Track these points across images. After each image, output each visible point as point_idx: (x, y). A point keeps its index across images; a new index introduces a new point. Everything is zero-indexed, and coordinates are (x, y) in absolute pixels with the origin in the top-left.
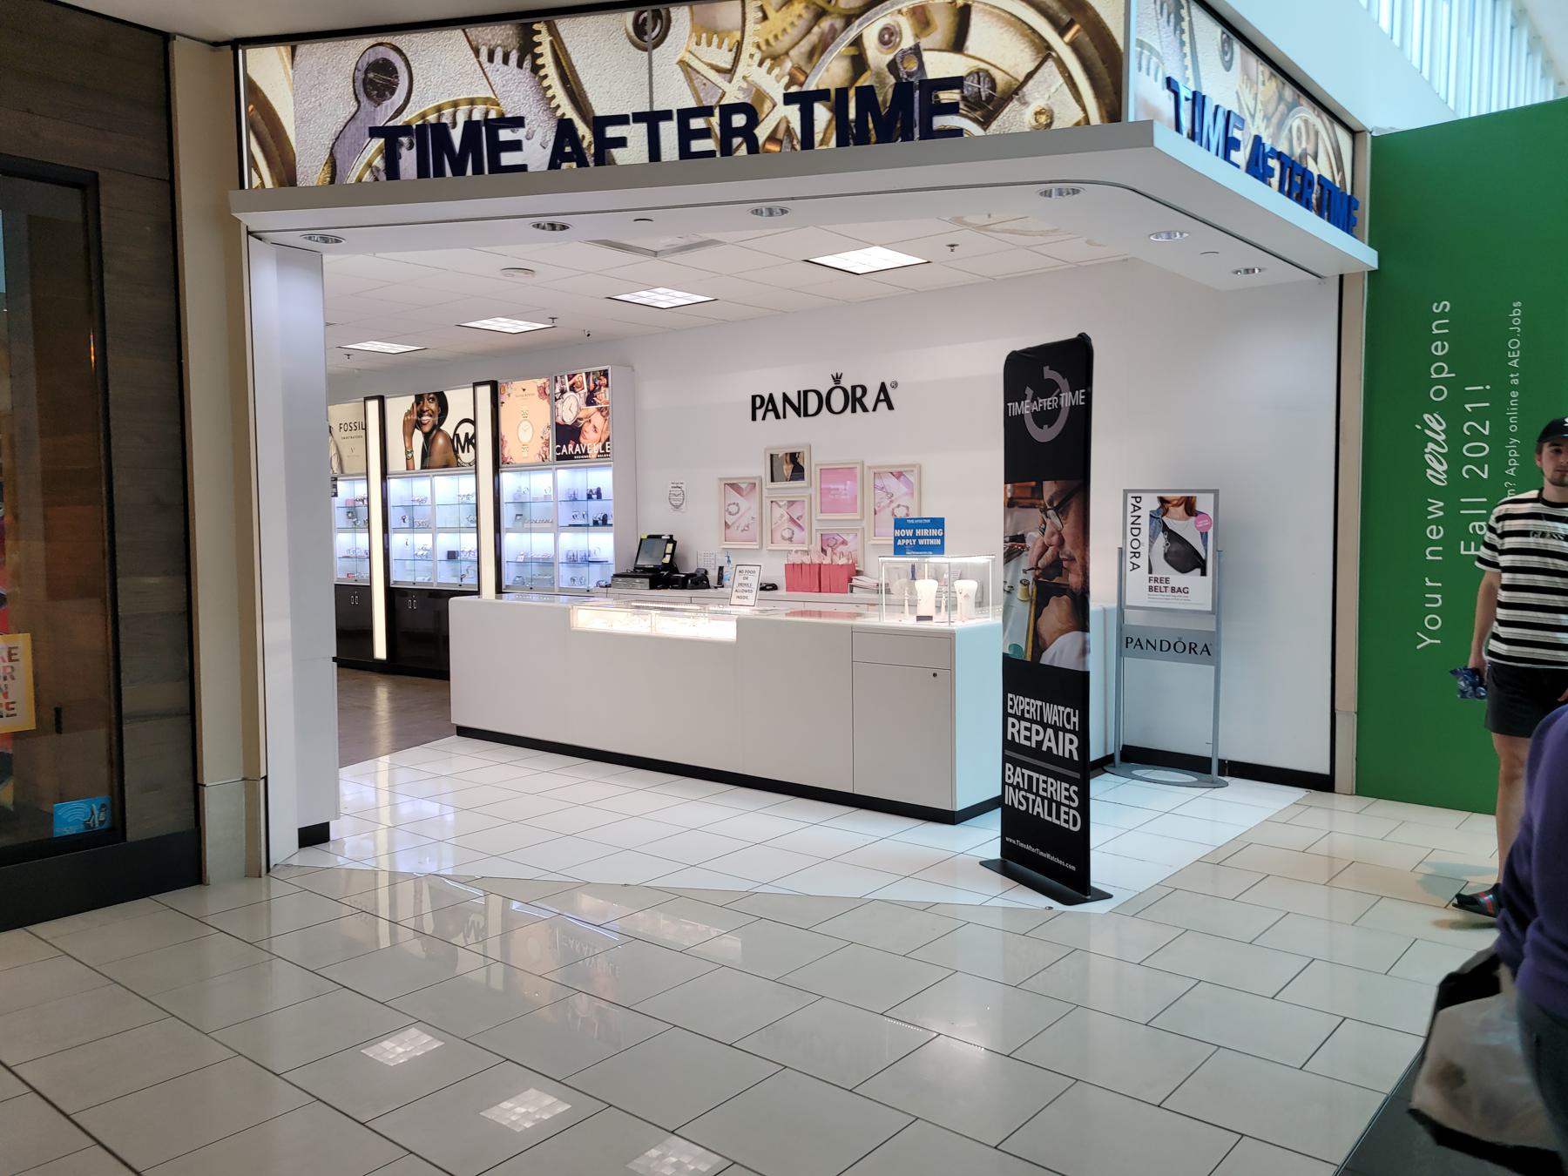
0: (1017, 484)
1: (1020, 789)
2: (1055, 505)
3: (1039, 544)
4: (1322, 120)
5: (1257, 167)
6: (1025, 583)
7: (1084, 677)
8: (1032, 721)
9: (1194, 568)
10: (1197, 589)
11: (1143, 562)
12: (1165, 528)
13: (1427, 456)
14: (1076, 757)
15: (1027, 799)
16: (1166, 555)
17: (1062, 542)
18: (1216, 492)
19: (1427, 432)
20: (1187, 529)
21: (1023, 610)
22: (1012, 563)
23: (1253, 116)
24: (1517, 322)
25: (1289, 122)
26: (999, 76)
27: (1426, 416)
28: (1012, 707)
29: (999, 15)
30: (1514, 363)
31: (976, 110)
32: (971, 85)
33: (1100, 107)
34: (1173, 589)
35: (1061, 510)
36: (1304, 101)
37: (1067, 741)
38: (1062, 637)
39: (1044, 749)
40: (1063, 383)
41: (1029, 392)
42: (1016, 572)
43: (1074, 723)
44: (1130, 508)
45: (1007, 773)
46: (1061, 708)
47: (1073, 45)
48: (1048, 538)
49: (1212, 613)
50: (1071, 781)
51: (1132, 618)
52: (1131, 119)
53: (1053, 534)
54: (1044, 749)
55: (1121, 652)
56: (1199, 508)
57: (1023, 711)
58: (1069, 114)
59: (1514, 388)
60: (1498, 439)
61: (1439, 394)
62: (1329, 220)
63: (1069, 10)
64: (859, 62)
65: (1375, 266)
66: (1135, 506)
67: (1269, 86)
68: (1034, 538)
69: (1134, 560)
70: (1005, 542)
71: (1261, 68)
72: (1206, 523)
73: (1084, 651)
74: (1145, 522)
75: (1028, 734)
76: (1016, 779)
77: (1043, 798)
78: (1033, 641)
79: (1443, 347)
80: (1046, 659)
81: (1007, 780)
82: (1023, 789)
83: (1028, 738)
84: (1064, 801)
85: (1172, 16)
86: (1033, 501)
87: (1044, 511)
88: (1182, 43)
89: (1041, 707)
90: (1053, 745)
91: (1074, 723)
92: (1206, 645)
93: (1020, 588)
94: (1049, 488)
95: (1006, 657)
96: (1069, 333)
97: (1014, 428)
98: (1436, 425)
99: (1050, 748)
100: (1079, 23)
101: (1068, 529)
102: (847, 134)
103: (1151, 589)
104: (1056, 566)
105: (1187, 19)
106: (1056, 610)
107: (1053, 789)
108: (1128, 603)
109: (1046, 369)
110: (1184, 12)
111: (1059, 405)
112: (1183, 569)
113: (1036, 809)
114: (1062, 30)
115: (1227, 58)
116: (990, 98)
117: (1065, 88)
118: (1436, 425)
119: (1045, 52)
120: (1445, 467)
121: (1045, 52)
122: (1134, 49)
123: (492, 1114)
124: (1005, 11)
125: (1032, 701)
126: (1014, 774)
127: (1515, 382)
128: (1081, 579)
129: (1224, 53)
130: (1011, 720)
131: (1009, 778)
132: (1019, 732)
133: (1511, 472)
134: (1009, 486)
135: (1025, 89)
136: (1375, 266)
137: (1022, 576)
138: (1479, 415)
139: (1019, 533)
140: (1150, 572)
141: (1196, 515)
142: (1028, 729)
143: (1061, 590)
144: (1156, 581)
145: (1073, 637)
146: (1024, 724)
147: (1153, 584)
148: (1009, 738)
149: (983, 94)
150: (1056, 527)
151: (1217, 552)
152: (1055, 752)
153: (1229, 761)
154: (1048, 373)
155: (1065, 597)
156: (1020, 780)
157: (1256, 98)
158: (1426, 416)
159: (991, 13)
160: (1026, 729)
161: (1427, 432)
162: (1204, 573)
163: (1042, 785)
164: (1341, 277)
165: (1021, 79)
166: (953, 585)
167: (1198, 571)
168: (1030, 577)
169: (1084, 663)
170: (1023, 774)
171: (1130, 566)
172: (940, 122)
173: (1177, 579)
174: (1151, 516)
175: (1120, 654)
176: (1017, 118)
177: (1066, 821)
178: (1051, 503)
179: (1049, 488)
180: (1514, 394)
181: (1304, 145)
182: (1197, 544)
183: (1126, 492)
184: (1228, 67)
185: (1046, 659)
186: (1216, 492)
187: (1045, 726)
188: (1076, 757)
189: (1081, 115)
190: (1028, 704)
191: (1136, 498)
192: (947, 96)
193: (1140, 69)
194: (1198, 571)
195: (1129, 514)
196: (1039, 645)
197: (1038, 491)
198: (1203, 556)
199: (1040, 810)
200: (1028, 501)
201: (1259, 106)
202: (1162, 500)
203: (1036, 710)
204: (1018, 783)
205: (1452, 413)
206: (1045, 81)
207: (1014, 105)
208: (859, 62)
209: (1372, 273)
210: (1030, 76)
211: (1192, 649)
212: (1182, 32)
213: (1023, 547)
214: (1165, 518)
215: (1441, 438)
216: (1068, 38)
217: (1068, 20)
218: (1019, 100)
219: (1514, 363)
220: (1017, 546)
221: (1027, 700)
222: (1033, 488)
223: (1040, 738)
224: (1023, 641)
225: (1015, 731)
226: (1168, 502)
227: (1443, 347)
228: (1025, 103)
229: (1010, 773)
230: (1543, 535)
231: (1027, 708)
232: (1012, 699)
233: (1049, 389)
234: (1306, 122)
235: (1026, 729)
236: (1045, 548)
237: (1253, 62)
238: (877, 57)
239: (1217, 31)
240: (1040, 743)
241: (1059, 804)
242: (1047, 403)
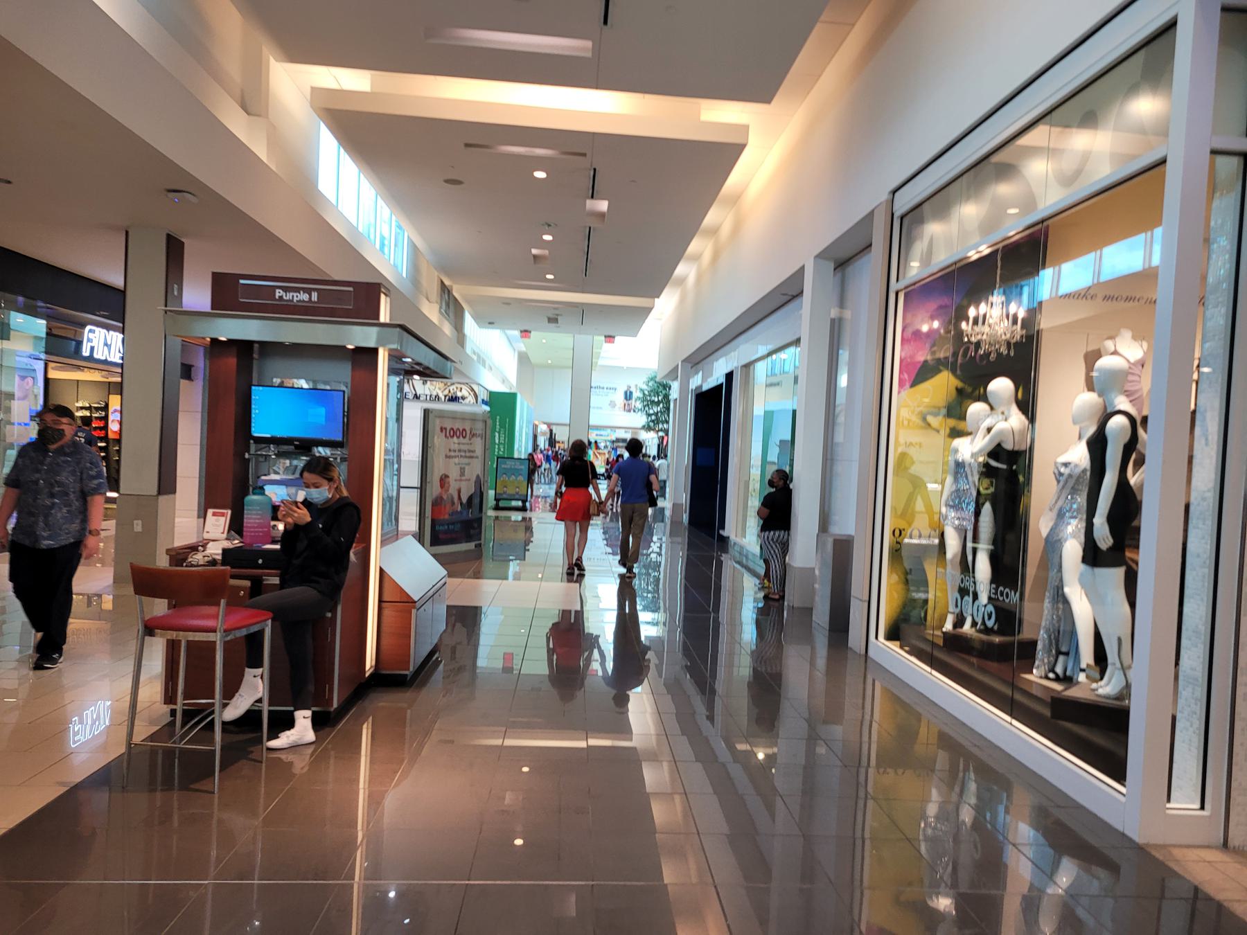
61: (497, 430)
64: (450, 392)
98: (497, 434)
102: (449, 400)
123: (356, 561)
166: (607, 470)
176: (467, 401)
205: (499, 433)
208: (450, 392)
213: (452, 515)
238: (452, 391)
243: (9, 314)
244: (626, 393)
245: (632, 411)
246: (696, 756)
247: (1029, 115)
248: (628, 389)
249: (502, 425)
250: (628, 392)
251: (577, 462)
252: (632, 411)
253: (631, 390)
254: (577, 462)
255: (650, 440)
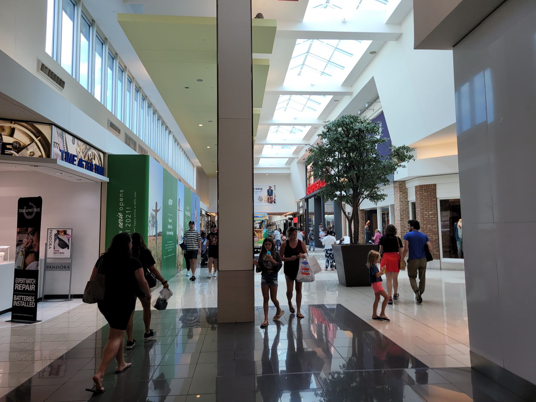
0: (21, 228)
1: (18, 301)
2: (31, 233)
3: (26, 242)
4: (96, 151)
5: (80, 164)
6: (22, 251)
7: (37, 271)
8: (22, 284)
9: (66, 247)
10: (66, 252)
11: (52, 246)
12: (59, 238)
13: (119, 222)
14: (34, 290)
15: (20, 303)
16: (58, 245)
17: (33, 241)
18: (72, 229)
19: (119, 217)
20: (64, 238)
21: (21, 258)
22: (19, 247)
23: (80, 153)
24: (135, 196)
25: (88, 153)
26: (21, 143)
27: (119, 213)
28: (17, 281)
29: (21, 131)
30: (135, 204)
31: (15, 149)
32: (15, 144)
33: (45, 153)
34: (60, 253)
35: (33, 234)
36: (92, 148)
37: (32, 287)
38: (32, 263)
39: (26, 289)
40: (34, 206)
41: (25, 207)
42: (20, 249)
43: (34, 282)
44: (49, 233)
45: (14, 298)
46: (31, 279)
47: (39, 140)
48: (29, 240)
49: (70, 258)
50: (32, 296)
51: (48, 261)
52: (52, 158)
53: (30, 240)
54: (26, 289)
55: (45, 270)
56: (67, 233)
57: (20, 282)
58: (38, 154)
59: (135, 209)
60: (132, 218)
61: (121, 209)
62: (97, 173)
63: (39, 134)
65: (108, 181)
66: (50, 232)
67: (83, 146)
68: (25, 240)
69: (50, 246)
70: (17, 242)
71: (81, 143)
72: (69, 236)
73: (38, 265)
74: (53, 237)
75: (21, 287)
76: (17, 299)
77: (25, 301)
78: (24, 265)
79: (122, 200)
80: (27, 268)
81: (14, 300)
82: (19, 301)
83: (21, 288)
84: (31, 301)
85: (61, 136)
86: (25, 232)
87: (28, 234)
88: (63, 141)
89: (25, 280)
90: (28, 288)
91: (34, 282)
92: (68, 266)
93: (21, 252)
94: (30, 229)
95: (15, 269)
96: (36, 195)
97: (20, 216)
98: (121, 215)
99: (27, 289)
100: (41, 137)
101: (35, 238)
103: (54, 253)
104: (31, 247)
105: (65, 136)
106: (30, 257)
107: (28, 299)
108: (48, 257)
109: (30, 203)
110: (64, 135)
111: (33, 211)
112: (63, 248)
113: (23, 305)
114: (37, 137)
115: (74, 142)
116: (19, 148)
117: (37, 148)
118: (121, 215)
119: (32, 141)
120: (122, 224)
121: (32, 141)
122: (53, 143)
124: (23, 131)
125: (23, 279)
126: (16, 298)
127: (135, 207)
128: (37, 249)
129: (73, 141)
130: (16, 285)
131: (15, 299)
132: (18, 287)
133: (135, 225)
134: (18, 229)
135: (28, 147)
136: (108, 181)
137: (21, 250)
138: (129, 214)
139: (21, 240)
140: (54, 249)
141: (67, 235)
142: (21, 286)
143: (32, 252)
144: (56, 251)
145: (35, 262)
146: (20, 285)
147: (55, 252)
148: (16, 289)
149: (17, 147)
150: (31, 238)
151: (72, 243)
152: (29, 290)
153: (74, 295)
154: (30, 204)
155: (33, 254)
156: (18, 299)
157: (80, 149)
158: (119, 213)
159: (20, 131)
160: (21, 286)
161: (119, 217)
162: (68, 249)
163: (25, 298)
164: (101, 182)
165: (27, 145)
167: (67, 248)
168: (24, 250)
169: (37, 268)
170: (19, 297)
171: (48, 248)
172: (7, 152)
173: (61, 250)
174: (55, 235)
175: (45, 270)
176: (26, 153)
177: (31, 305)
178: (30, 232)
179: (30, 229)
180: (135, 210)
181: (92, 157)
182: (67, 242)
183: (48, 229)
184: (74, 144)
185: (27, 268)
186: (72, 229)
187: (26, 284)
188: (34, 290)
189: (41, 154)
190: (22, 280)
191: (51, 230)
192: (8, 146)
193: (54, 147)
194: (67, 248)
195: (49, 235)
196: (25, 265)
197: (27, 230)
198: (68, 244)
199: (24, 305)
200: (24, 232)
201: (81, 150)
202: (58, 231)
203: (24, 281)
204: (18, 299)
206: (33, 146)
207: (25, 150)
209: (108, 182)
210: (29, 145)
211: (65, 267)
212: (64, 139)
214: (58, 236)
215: (122, 218)
216: (38, 139)
217: (38, 135)
218: (26, 149)
219: (135, 204)
220: (21, 243)
221: (21, 279)
222: (25, 229)
223: (24, 287)
224: (21, 265)
225: (17, 287)
226: (60, 231)
227: (122, 200)
228: (28, 150)
229: (15, 298)
230: (192, 235)
231: (21, 281)
232: (17, 279)
233: (31, 207)
234: (92, 152)
235: (21, 286)
236: (28, 243)
237: (80, 142)
239: (71, 137)
240: (24, 289)
241: (29, 302)
242: (30, 210)
243: (136, 311)
244: (268, 191)
245: (273, 202)
246: (340, 329)
247: (376, 113)
248: (270, 189)
249: (128, 202)
250: (270, 190)
251: (390, 237)
252: (273, 202)
253: (271, 189)
254: (390, 237)
255: (279, 222)
